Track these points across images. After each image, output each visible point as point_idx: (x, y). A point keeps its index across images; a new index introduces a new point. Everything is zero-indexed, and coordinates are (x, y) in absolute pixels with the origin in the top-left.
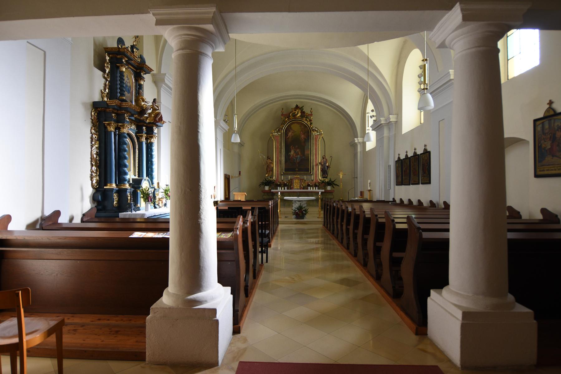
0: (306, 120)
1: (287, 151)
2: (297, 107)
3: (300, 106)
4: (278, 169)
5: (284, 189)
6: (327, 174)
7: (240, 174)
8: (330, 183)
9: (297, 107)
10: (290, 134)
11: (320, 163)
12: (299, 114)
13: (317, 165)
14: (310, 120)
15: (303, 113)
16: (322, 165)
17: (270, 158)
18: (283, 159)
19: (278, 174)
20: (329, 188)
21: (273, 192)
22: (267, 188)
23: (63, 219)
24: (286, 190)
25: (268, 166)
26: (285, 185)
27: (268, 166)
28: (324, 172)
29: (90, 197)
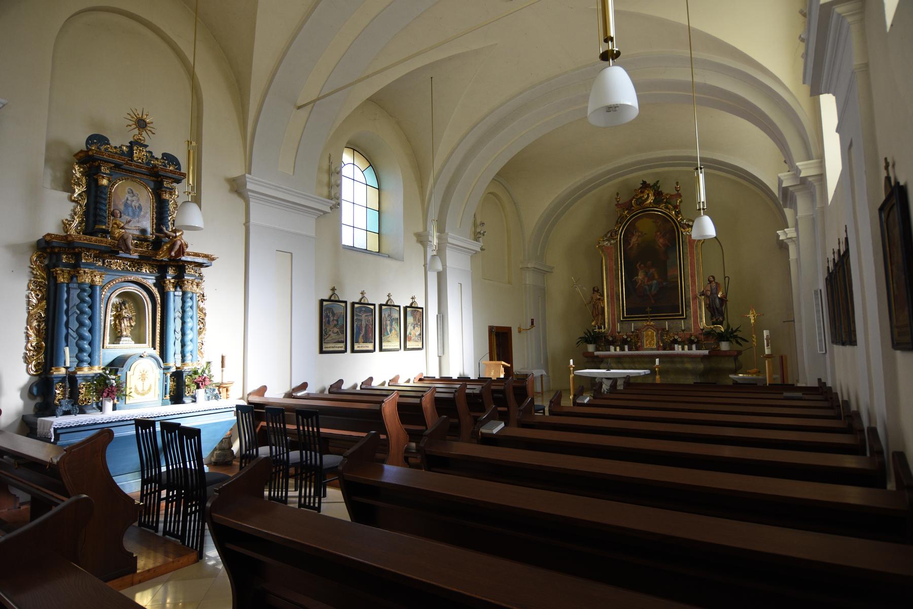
0: (667, 208)
1: (631, 273)
2: (645, 185)
3: (650, 181)
4: (613, 310)
5: (622, 349)
6: (722, 314)
7: (532, 323)
8: (728, 336)
9: (645, 185)
10: (634, 240)
11: (703, 294)
12: (651, 199)
13: (695, 298)
14: (675, 207)
15: (658, 194)
16: (707, 296)
17: (597, 290)
18: (622, 290)
19: (613, 320)
20: (724, 346)
21: (597, 357)
22: (591, 348)
23: (345, 387)
24: (627, 351)
25: (595, 306)
26: (623, 342)
27: (594, 305)
28: (716, 310)
29: (22, 390)
